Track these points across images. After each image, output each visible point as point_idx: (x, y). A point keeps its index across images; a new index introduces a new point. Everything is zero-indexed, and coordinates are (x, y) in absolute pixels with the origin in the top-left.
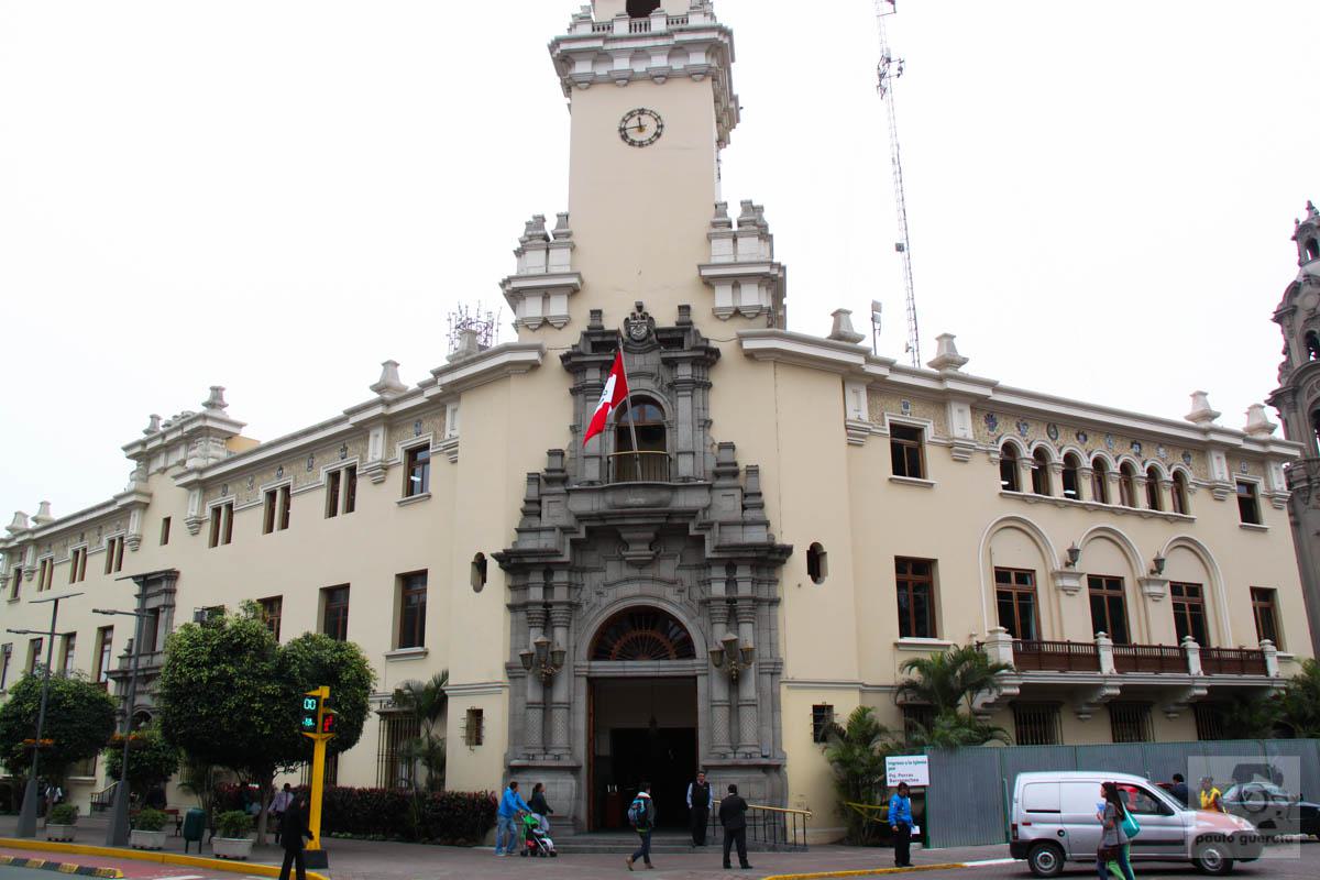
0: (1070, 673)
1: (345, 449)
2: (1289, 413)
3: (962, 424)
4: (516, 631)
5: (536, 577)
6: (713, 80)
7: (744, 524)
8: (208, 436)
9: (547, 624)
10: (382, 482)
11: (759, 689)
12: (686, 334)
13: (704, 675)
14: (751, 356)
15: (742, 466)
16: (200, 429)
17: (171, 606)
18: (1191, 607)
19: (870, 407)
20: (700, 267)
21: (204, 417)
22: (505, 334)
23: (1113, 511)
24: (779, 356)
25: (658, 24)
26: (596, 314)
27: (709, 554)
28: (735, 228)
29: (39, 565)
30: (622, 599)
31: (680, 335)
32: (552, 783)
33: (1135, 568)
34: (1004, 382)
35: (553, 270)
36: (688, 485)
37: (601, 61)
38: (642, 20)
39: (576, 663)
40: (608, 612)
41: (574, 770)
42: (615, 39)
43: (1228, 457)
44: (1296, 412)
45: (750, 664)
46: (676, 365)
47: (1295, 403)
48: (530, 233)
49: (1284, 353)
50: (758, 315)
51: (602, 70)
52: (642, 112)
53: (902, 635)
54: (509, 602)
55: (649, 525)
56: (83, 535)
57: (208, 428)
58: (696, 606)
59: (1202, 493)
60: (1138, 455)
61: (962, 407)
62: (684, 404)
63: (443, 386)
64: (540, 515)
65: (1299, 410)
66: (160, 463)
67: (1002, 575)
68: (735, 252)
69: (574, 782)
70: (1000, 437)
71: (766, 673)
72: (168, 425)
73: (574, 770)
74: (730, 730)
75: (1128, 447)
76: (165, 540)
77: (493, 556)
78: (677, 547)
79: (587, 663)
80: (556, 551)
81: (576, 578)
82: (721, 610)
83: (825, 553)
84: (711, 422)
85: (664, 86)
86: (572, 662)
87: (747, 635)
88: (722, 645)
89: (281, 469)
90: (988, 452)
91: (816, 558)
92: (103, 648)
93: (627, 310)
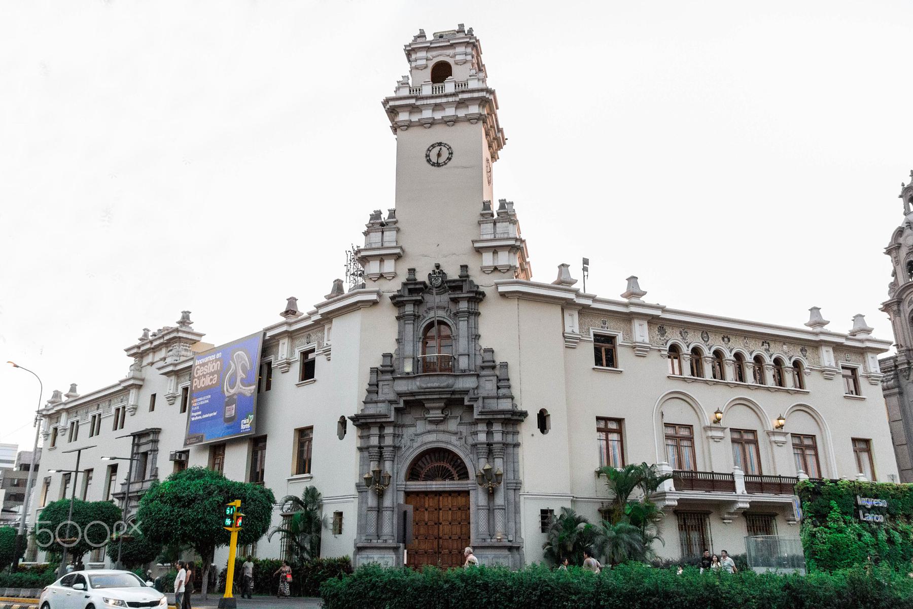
0: (713, 493)
2: (895, 317)
3: (641, 332)
4: (363, 463)
5: (375, 431)
6: (483, 123)
7: (498, 398)
8: (180, 342)
9: (381, 458)
10: (287, 372)
11: (506, 498)
13: (473, 490)
14: (503, 295)
15: (498, 363)
16: (175, 338)
17: (155, 451)
19: (580, 324)
20: (473, 242)
21: (177, 330)
23: (748, 387)
25: (449, 87)
27: (476, 416)
28: (496, 216)
29: (69, 425)
31: (460, 284)
33: (764, 422)
34: (669, 307)
35: (386, 245)
36: (464, 374)
37: (414, 112)
38: (440, 85)
39: (398, 483)
40: (417, 451)
42: (423, 98)
43: (835, 350)
45: (500, 483)
46: (459, 302)
47: (899, 310)
48: (372, 222)
49: (893, 276)
50: (508, 270)
51: (415, 118)
52: (440, 144)
54: (359, 445)
56: (99, 405)
57: (180, 338)
58: (469, 447)
60: (767, 350)
61: (641, 322)
62: (463, 325)
64: (377, 393)
65: (902, 315)
66: (149, 359)
68: (495, 233)
69: (394, 557)
70: (667, 341)
71: (511, 489)
72: (154, 335)
74: (489, 523)
75: (760, 344)
76: (152, 408)
77: (349, 418)
78: (458, 412)
79: (404, 483)
80: (386, 415)
81: (399, 431)
82: (483, 450)
84: (480, 336)
85: (453, 127)
86: (395, 483)
87: (498, 465)
88: (482, 472)
90: (659, 350)
91: (543, 420)
92: (111, 478)
93: (430, 268)
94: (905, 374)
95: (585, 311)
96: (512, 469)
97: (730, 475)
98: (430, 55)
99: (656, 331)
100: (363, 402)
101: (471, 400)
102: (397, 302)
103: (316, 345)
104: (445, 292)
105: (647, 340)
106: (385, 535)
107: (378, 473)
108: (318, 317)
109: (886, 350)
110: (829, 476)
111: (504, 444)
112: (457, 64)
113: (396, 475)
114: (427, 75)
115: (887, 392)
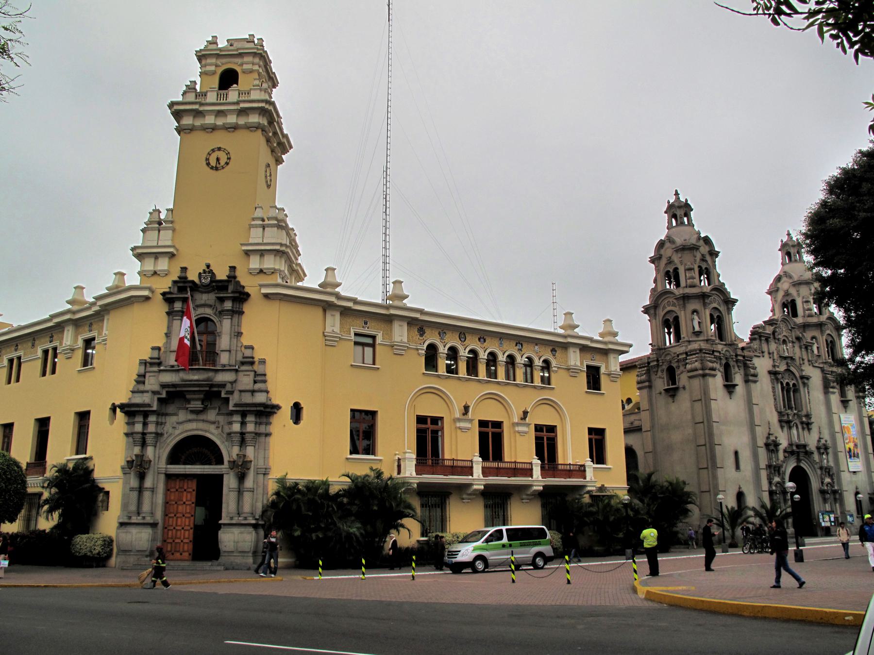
1: (52, 337)
3: (400, 333)
4: (128, 448)
5: (140, 419)
6: (262, 131)
9: (144, 444)
12: (230, 284)
13: (227, 474)
14: (267, 296)
15: (256, 359)
18: (548, 439)
22: (133, 279)
24: (282, 297)
25: (233, 94)
26: (184, 269)
27: (231, 408)
30: (187, 431)
31: (226, 284)
32: (139, 532)
39: (159, 466)
41: (154, 525)
44: (656, 319)
50: (273, 273)
51: (198, 122)
53: (351, 453)
55: (199, 391)
58: (225, 436)
59: (563, 373)
63: (100, 306)
64: (144, 383)
65: (657, 317)
67: (421, 420)
73: (154, 525)
78: (217, 403)
82: (237, 438)
83: (302, 408)
89: (17, 346)
90: (417, 349)
91: (297, 411)
93: (202, 267)
94: (654, 370)
95: (346, 312)
96: (263, 456)
97: (470, 461)
98: (219, 62)
99: (415, 332)
100: (131, 391)
101: (228, 392)
102: (168, 298)
103: (96, 334)
104: (213, 290)
105: (405, 340)
106: (144, 513)
107: (140, 457)
108: (96, 308)
109: (627, 352)
110: (564, 461)
111: (256, 434)
112: (244, 72)
113: (157, 459)
114: (215, 81)
115: (640, 385)
